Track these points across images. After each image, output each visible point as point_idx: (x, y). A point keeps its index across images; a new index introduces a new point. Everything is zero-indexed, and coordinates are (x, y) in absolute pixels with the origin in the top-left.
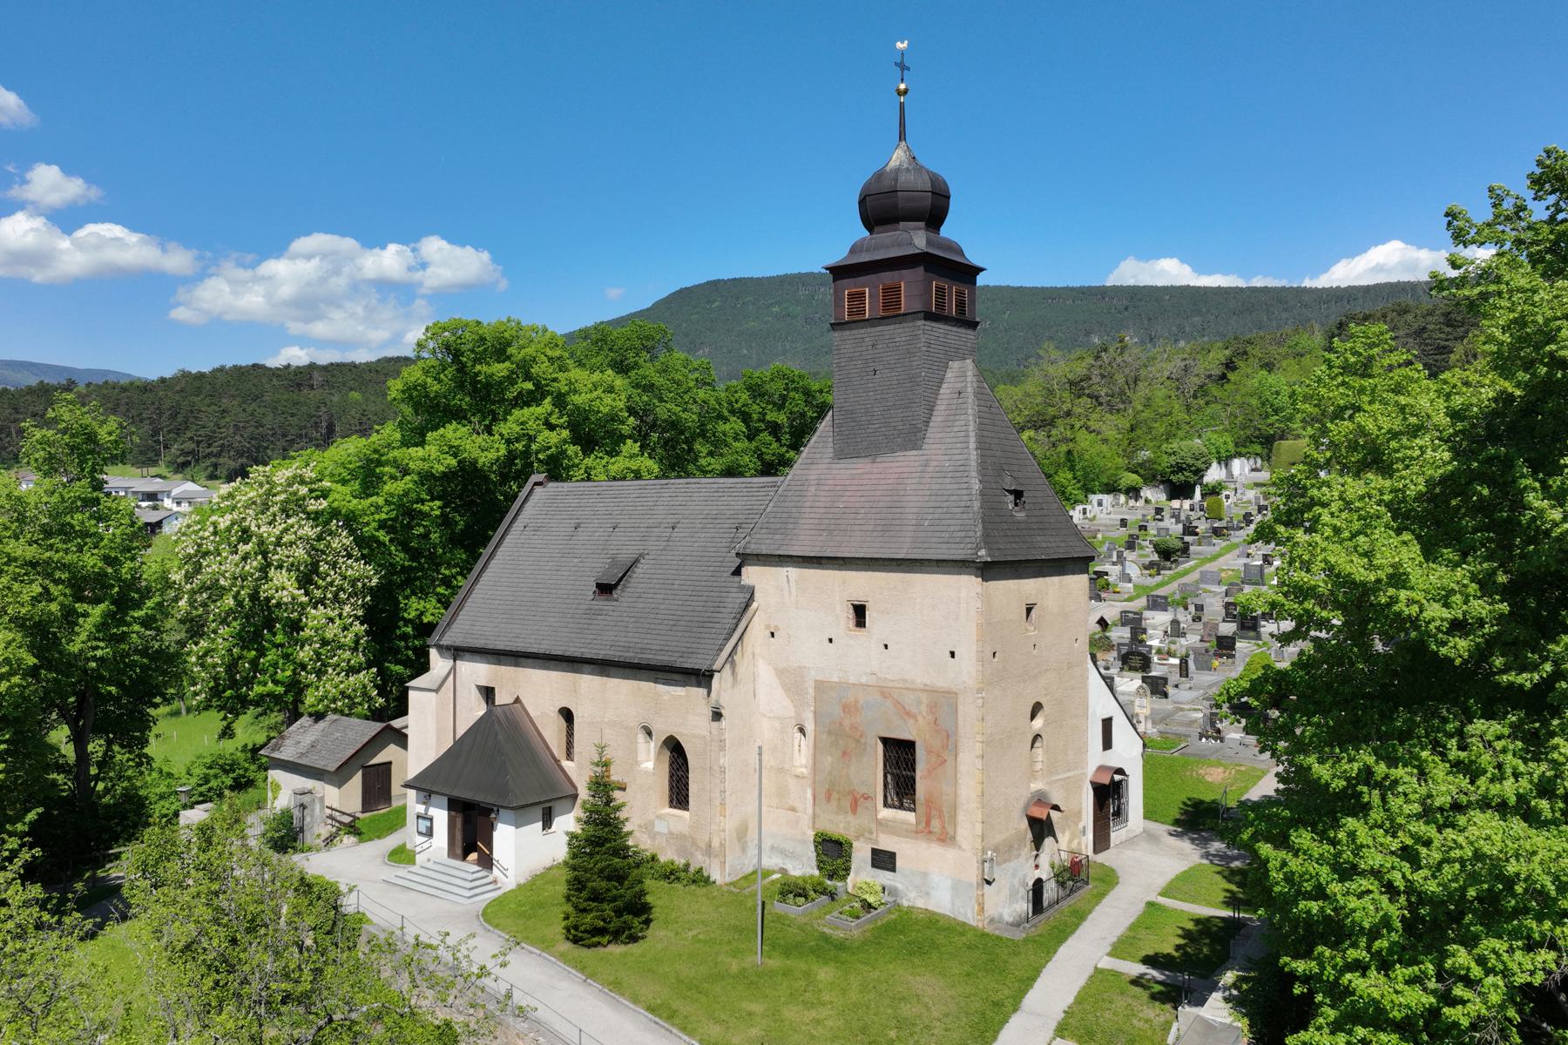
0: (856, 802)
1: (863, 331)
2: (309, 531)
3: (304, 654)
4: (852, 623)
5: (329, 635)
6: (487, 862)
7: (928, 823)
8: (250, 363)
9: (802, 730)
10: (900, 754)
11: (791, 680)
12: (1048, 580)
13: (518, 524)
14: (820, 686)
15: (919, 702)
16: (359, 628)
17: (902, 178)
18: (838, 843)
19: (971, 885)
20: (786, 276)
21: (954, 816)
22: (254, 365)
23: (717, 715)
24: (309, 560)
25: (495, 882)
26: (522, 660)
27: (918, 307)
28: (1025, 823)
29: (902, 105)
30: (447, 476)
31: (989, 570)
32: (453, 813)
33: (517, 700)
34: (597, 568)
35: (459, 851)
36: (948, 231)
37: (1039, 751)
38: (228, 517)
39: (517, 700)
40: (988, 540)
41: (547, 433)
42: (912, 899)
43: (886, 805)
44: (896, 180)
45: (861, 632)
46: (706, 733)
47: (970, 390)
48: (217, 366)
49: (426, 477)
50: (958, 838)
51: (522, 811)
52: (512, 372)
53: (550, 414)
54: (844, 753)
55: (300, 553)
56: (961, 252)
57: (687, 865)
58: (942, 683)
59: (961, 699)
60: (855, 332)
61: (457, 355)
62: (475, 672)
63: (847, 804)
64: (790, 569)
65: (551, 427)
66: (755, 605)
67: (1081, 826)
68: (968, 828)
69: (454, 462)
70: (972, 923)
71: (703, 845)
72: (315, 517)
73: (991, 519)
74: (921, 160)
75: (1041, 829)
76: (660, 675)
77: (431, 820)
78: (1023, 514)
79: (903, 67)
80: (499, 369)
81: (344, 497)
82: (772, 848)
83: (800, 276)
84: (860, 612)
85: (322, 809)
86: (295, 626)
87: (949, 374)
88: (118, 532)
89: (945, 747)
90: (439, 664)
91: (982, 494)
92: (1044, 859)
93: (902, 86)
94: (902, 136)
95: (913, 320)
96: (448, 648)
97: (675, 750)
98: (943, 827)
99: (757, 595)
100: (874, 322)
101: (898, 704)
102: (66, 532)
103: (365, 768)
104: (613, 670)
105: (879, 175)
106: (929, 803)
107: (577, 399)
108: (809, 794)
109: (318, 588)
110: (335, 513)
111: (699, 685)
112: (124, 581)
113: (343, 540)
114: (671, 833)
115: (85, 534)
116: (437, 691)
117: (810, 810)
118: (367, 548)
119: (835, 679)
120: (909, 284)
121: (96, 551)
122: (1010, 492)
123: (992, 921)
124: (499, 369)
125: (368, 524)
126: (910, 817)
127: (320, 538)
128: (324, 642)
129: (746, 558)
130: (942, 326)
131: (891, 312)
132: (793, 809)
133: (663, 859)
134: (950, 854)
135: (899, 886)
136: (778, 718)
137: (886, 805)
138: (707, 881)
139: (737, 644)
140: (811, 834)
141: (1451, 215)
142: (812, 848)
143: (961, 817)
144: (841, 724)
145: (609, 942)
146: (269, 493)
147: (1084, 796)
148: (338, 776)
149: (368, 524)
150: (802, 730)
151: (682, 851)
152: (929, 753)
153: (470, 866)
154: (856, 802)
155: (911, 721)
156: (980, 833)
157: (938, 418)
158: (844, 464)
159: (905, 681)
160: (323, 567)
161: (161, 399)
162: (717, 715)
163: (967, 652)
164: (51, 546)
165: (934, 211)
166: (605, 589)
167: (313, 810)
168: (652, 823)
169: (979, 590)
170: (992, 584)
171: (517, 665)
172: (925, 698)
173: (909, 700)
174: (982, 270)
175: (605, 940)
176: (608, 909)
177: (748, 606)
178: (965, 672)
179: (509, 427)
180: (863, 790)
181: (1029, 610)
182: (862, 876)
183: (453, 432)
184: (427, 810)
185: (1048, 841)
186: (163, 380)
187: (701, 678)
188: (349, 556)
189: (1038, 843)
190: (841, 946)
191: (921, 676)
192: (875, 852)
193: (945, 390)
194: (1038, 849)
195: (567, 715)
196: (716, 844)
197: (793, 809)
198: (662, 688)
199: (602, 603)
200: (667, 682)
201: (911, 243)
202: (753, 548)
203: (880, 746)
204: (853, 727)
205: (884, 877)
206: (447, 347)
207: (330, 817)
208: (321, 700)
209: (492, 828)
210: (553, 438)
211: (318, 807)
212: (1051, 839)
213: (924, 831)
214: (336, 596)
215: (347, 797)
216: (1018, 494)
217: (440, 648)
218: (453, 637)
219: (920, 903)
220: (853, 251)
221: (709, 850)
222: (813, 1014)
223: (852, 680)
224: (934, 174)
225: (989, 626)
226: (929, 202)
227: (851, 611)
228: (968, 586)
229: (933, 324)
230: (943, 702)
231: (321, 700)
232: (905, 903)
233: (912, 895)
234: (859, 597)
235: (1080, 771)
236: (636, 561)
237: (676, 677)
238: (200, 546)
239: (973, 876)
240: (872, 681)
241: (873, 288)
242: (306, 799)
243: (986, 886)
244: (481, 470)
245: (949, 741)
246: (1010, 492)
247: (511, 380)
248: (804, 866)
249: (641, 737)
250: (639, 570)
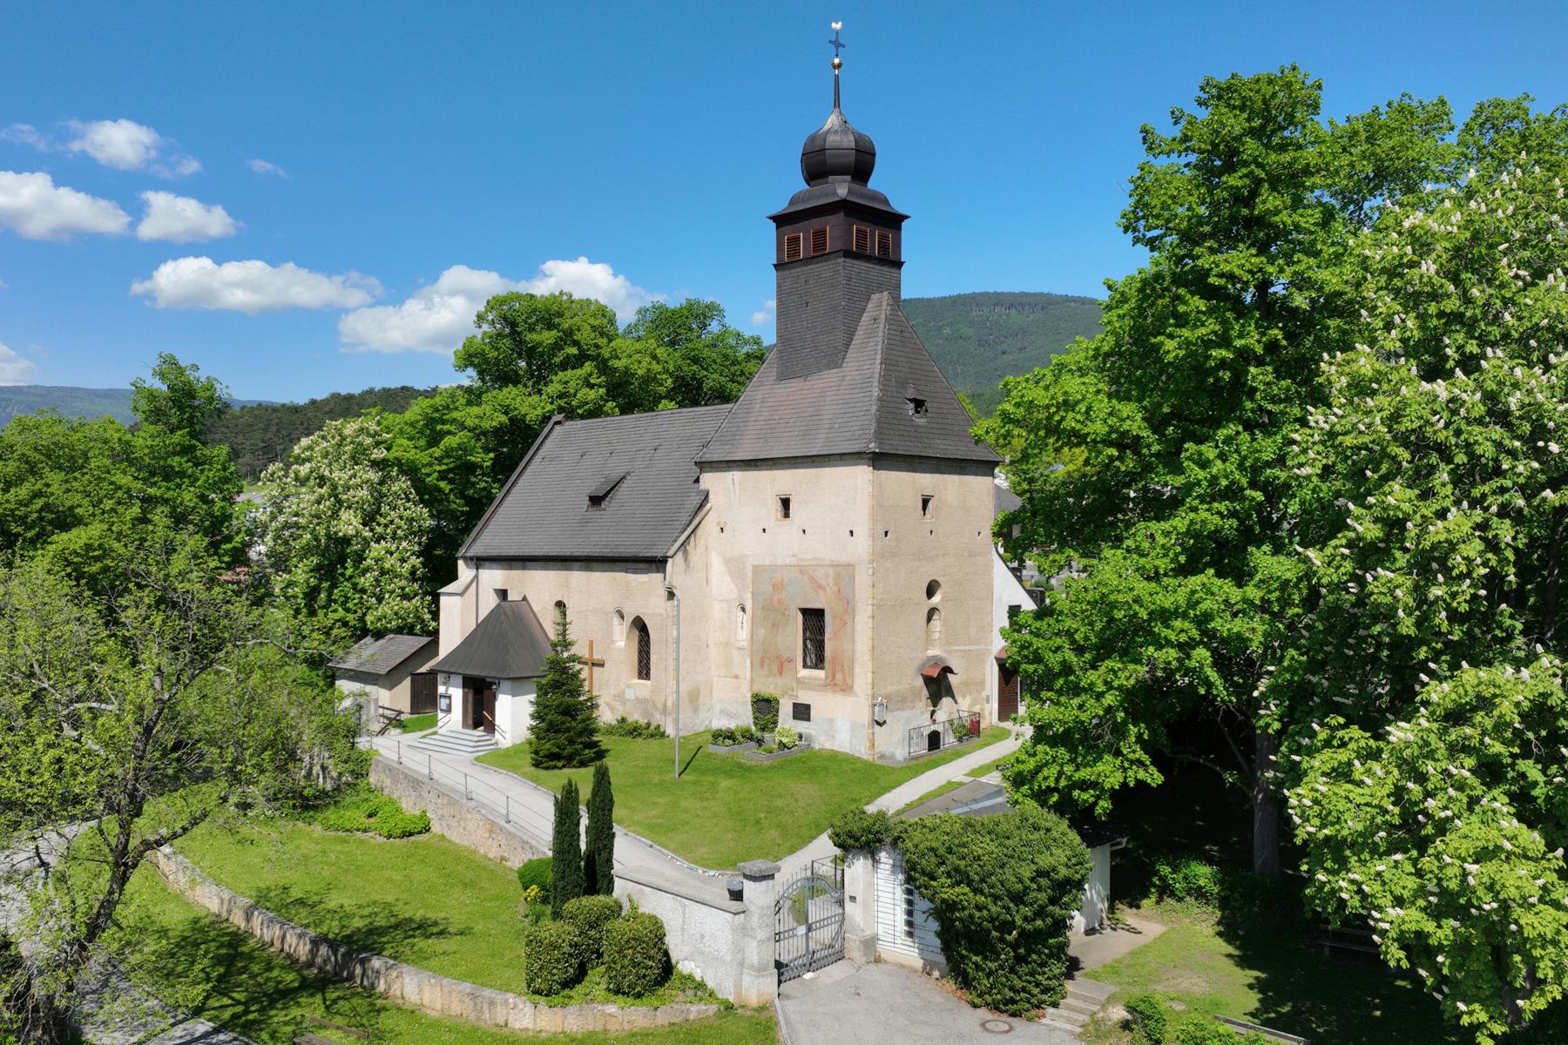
0: (782, 665)
2: (374, 476)
3: (366, 581)
4: (780, 514)
5: (387, 565)
6: (491, 728)
7: (834, 677)
8: (399, 385)
9: (743, 610)
10: (814, 618)
11: (734, 566)
12: (947, 477)
13: (538, 458)
14: (757, 570)
15: (827, 575)
16: (415, 561)
17: (831, 138)
18: (768, 701)
19: (863, 726)
20: (959, 296)
21: (852, 669)
22: (403, 388)
23: (671, 595)
24: (372, 501)
25: (497, 743)
26: (528, 564)
27: (839, 246)
28: (920, 681)
29: (837, 77)
30: (498, 431)
31: (879, 460)
33: (524, 599)
34: (594, 485)
35: (470, 722)
36: (874, 183)
37: (936, 623)
38: (308, 465)
39: (524, 599)
40: (879, 435)
41: (585, 390)
42: (822, 742)
43: (805, 666)
44: (825, 140)
46: (663, 611)
47: (883, 316)
48: (366, 388)
49: (478, 433)
50: (855, 687)
51: (518, 683)
52: (561, 339)
53: (590, 375)
54: (774, 625)
55: (364, 493)
56: (886, 202)
57: (649, 725)
58: (844, 558)
59: (857, 570)
61: (513, 325)
62: (493, 577)
63: (775, 668)
65: (592, 386)
66: (709, 506)
67: (984, 694)
68: (862, 679)
69: (504, 419)
70: (865, 757)
71: (660, 706)
72: (375, 464)
73: (886, 419)
74: (852, 124)
75: (938, 685)
76: (629, 565)
77: (450, 697)
78: (924, 420)
79: (837, 44)
80: (547, 337)
81: (405, 449)
82: (721, 711)
83: (974, 296)
85: (376, 709)
86: (360, 558)
87: (870, 305)
88: (211, 474)
89: (846, 611)
90: (465, 572)
91: (880, 399)
92: (941, 716)
93: (837, 61)
94: (837, 104)
96: (471, 559)
97: (640, 626)
98: (844, 678)
99: (711, 497)
100: (808, 260)
101: (813, 580)
102: (169, 475)
103: (414, 676)
104: (595, 565)
105: (812, 139)
106: (834, 659)
107: (618, 364)
108: (748, 663)
109: (379, 524)
110: (398, 462)
111: (658, 572)
112: (216, 517)
113: (402, 484)
114: (637, 699)
115: (182, 474)
116: (462, 594)
117: (749, 677)
118: (427, 494)
119: (767, 563)
120: (833, 227)
121: (192, 489)
122: (911, 400)
123: (882, 756)
124: (547, 337)
125: (429, 475)
126: (820, 674)
127: (382, 483)
128: (383, 572)
129: (704, 466)
130: (864, 264)
131: (819, 251)
132: (736, 677)
133: (630, 720)
135: (813, 732)
137: (805, 666)
138: (663, 735)
139: (689, 536)
140: (749, 695)
141: (1145, 131)
142: (750, 708)
143: (857, 670)
145: (564, 766)
146: (340, 445)
147: (988, 670)
148: (389, 679)
149: (429, 475)
150: (743, 610)
151: (645, 713)
152: (835, 617)
153: (480, 731)
154: (782, 665)
155: (822, 592)
156: (870, 681)
157: (856, 342)
158: (783, 384)
159: (818, 559)
160: (384, 509)
161: (309, 419)
162: (671, 595)
163: (862, 532)
164: (155, 483)
165: (861, 164)
166: (596, 501)
167: (369, 710)
168: (623, 692)
169: (871, 477)
170: (884, 474)
171: (524, 568)
172: (831, 572)
173: (820, 574)
174: (906, 217)
175: (560, 764)
176: (562, 739)
177: (701, 506)
178: (861, 547)
179: (553, 388)
180: (788, 655)
181: (925, 502)
182: (786, 723)
183: (510, 394)
185: (946, 702)
186: (313, 402)
187: (657, 563)
188: (408, 500)
189: (935, 699)
190: (750, 769)
191: (829, 554)
192: (795, 705)
193: (866, 318)
194: (935, 704)
195: (560, 605)
197: (736, 677)
198: (631, 577)
199: (595, 514)
200: (635, 571)
201: (835, 194)
202: (708, 457)
203: (800, 616)
204: (780, 602)
205: (801, 726)
206: (505, 318)
207: (383, 716)
208: (379, 620)
209: (494, 698)
210: (592, 395)
211: (372, 708)
212: (950, 699)
213: (832, 685)
214: (395, 533)
215: (399, 697)
216: (919, 404)
217: (465, 558)
218: (478, 549)
219: (828, 746)
220: (792, 202)
221: (665, 710)
222: (705, 804)
223: (780, 562)
224: (860, 135)
225: (879, 507)
226: (853, 158)
227: (780, 503)
228: (862, 474)
229: (854, 262)
230: (844, 573)
231: (379, 620)
232: (817, 747)
233: (822, 739)
234: (784, 492)
235: (982, 647)
236: (624, 478)
237: (641, 566)
238: (283, 489)
239: (866, 718)
240: (793, 561)
241: (806, 232)
242: (362, 700)
243: (877, 727)
244: (529, 426)
245: (848, 606)
246: (911, 400)
247: (557, 346)
248: (743, 718)
249: (616, 620)
250: (624, 485)
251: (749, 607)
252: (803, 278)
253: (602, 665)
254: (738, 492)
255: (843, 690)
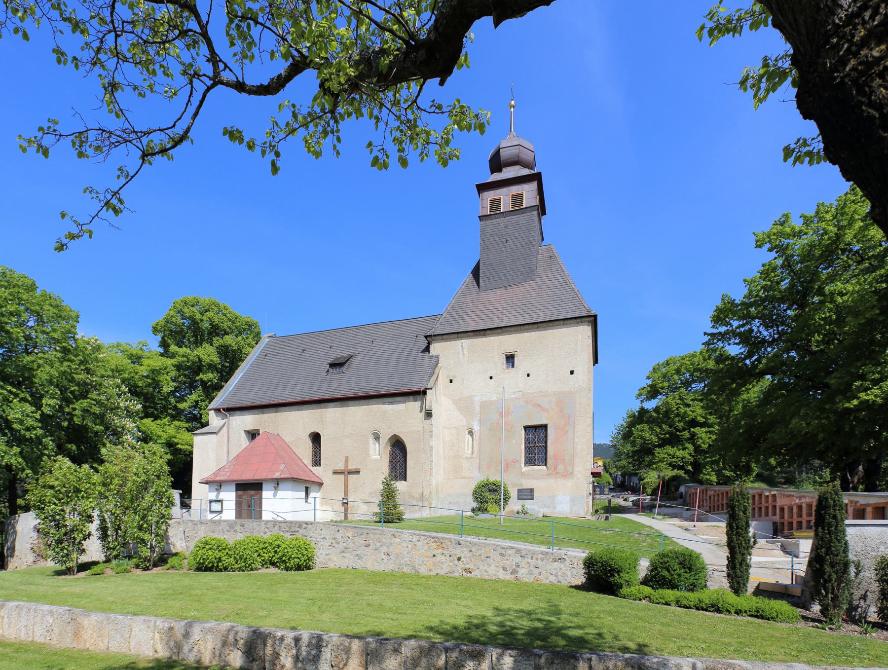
1: (499, 220)
9: (471, 433)
11: (464, 405)
14: (484, 405)
23: (429, 415)
32: (240, 493)
45: (511, 370)
60: (494, 221)
64: (463, 341)
84: (510, 359)
95: (531, 211)
134: (569, 483)
136: (455, 428)
144: (498, 423)
177: (437, 365)
184: (217, 496)
195: (316, 438)
196: (426, 493)
234: (509, 350)
236: (479, 287)
249: (371, 440)
251: (476, 428)
252: (502, 225)
253: (357, 472)
254: (466, 353)
255: (564, 476)
